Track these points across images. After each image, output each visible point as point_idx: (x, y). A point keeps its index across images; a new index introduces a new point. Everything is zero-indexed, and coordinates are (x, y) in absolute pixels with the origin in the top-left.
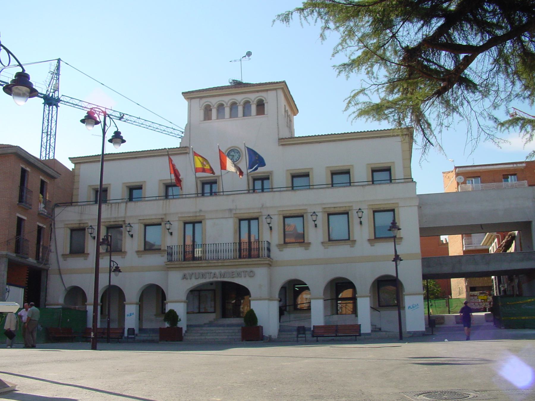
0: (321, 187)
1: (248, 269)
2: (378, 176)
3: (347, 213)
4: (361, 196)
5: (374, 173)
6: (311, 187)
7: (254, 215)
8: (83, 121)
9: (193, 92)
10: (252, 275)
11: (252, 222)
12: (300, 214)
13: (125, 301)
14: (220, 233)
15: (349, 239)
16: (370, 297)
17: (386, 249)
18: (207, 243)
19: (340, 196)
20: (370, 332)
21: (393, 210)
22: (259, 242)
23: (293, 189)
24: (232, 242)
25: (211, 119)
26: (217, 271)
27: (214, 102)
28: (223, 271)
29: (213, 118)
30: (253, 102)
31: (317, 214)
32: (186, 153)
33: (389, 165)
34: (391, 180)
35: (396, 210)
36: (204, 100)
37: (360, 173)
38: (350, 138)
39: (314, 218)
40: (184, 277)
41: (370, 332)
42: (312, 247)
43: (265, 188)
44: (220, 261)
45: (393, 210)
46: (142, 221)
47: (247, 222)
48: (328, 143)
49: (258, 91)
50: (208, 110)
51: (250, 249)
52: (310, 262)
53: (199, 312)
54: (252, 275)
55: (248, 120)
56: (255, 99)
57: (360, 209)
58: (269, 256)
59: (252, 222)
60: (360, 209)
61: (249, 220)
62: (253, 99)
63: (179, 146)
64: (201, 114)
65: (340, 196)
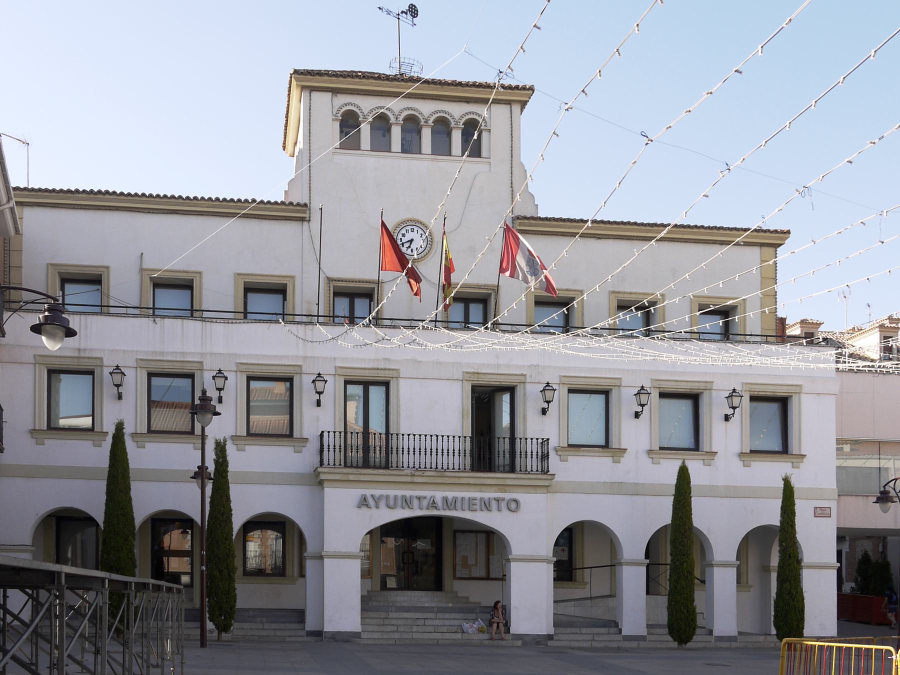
0: (126, 311)
1: (508, 496)
2: (258, 302)
3: (606, 393)
5: (250, 295)
6: (105, 309)
7: (382, 376)
9: (319, 73)
10: (514, 506)
11: (373, 390)
14: (434, 414)
15: (290, 435)
16: (712, 565)
17: (771, 473)
18: (529, 436)
19: (269, 343)
21: (606, 393)
22: (346, 433)
23: (245, 317)
25: (358, 148)
26: (439, 495)
27: (366, 106)
29: (363, 147)
30: (457, 123)
31: (226, 374)
32: (302, 219)
36: (342, 99)
37: (219, 291)
38: (560, 230)
39: (117, 378)
40: (363, 502)
42: (627, 459)
44: (447, 474)
45: (290, 380)
46: (243, 368)
48: (692, 244)
49: (468, 100)
50: (349, 122)
51: (366, 448)
52: (617, 488)
54: (514, 506)
55: (443, 164)
56: (371, 111)
58: (545, 471)
59: (373, 390)
61: (366, 385)
62: (457, 118)
63: (280, 198)
64: (330, 131)
65: (269, 343)
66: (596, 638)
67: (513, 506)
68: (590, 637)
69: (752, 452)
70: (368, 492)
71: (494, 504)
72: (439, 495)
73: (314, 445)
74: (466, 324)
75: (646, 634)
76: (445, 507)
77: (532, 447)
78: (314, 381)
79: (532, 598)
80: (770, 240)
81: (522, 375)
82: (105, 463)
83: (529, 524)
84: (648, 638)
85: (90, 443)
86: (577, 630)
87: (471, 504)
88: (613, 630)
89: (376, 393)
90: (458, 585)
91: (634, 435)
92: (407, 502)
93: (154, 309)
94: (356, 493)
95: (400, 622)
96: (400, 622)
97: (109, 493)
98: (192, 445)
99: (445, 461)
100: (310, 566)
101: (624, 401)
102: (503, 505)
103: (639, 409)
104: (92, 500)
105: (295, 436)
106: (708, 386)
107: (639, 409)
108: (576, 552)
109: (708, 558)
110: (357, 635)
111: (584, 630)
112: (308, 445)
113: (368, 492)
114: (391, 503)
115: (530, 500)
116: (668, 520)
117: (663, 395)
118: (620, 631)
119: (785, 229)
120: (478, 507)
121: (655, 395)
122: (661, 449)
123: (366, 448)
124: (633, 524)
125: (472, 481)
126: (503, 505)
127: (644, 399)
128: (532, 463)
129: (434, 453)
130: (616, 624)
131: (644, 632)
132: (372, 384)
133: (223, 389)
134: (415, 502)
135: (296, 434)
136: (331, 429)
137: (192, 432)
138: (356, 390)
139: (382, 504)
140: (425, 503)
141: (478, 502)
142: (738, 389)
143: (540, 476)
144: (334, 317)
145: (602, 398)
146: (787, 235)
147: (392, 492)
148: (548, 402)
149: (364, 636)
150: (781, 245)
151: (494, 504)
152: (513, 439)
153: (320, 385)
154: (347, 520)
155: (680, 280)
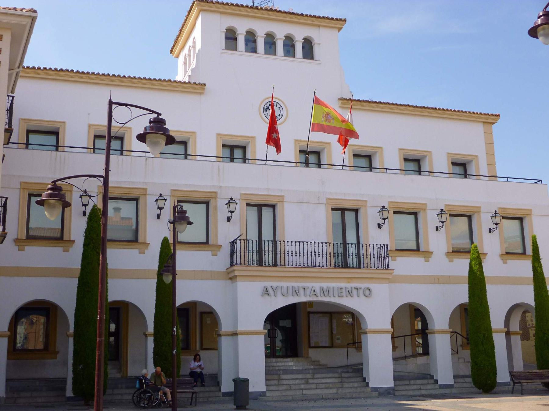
3: (137, 200)
4: (437, 191)
8: (533, 32)
11: (264, 210)
12: (202, 199)
13: (427, 329)
14: (305, 226)
18: (286, 240)
20: (391, 384)
21: (521, 219)
24: (332, 242)
26: (317, 285)
28: (325, 285)
33: (55, 125)
34: (186, 156)
35: (141, 202)
41: (391, 384)
43: (125, 148)
47: (256, 208)
53: (332, 346)
57: (161, 195)
59: (264, 210)
60: (161, 195)
61: (260, 207)
66: (422, 388)
67: (367, 292)
68: (418, 387)
69: (397, 250)
70: (268, 284)
71: (355, 292)
72: (317, 285)
73: (226, 250)
74: (307, 164)
75: (453, 383)
76: (322, 294)
77: (374, 251)
78: (157, 200)
79: (379, 359)
80: (489, 120)
81: (143, 189)
82: (531, 274)
83: (376, 307)
84: (456, 385)
85: (60, 249)
86: (407, 382)
87: (340, 292)
88: (432, 381)
89: (267, 214)
90: (313, 353)
91: (437, 242)
92: (296, 292)
93: (94, 149)
94: (258, 286)
95: (291, 382)
96: (291, 382)
97: (536, 290)
98: (210, 252)
99: (319, 260)
100: (225, 343)
101: (430, 219)
102: (361, 292)
103: (229, 215)
104: (64, 295)
105: (527, 253)
106: (424, 207)
107: (229, 215)
108: (412, 324)
109: (363, 327)
110: (264, 394)
111: (412, 382)
112: (222, 250)
113: (268, 284)
114: (285, 291)
115: (380, 290)
116: (465, 299)
117: (395, 212)
118: (436, 382)
119: (497, 114)
120: (344, 294)
121: (391, 212)
122: (453, 252)
123: (260, 252)
124: (442, 304)
125: (375, 276)
126: (361, 292)
127: (232, 207)
128: (374, 261)
129: (294, 254)
130: (432, 377)
131: (452, 382)
132: (264, 207)
133: (87, 205)
134: (302, 291)
135: (66, 238)
136: (325, 241)
137: (524, 253)
138: (253, 211)
139: (279, 293)
140: (308, 292)
141: (344, 290)
142: (386, 206)
143: (244, 268)
144: (266, 160)
145: (204, 206)
146: (498, 117)
147: (285, 284)
148: (232, 212)
149: (268, 394)
150: (494, 123)
151: (355, 292)
152: (275, 242)
153: (161, 203)
154: (246, 308)
155: (441, 141)
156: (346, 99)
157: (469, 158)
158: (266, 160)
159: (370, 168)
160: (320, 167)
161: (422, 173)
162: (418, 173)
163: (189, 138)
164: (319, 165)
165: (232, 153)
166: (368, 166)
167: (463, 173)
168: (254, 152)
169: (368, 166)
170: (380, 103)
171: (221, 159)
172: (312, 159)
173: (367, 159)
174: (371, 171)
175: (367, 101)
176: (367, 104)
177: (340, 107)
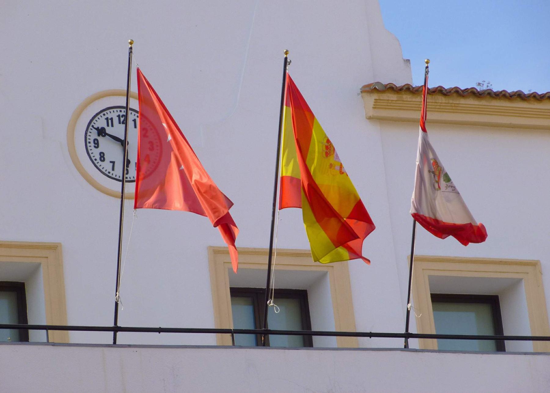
74: (261, 336)
156: (391, 89)
157: (510, 273)
158: (116, 329)
159: (499, 341)
160: (308, 344)
161: (316, 339)
162: (491, 344)
163: (35, 270)
164: (306, 336)
165: (260, 314)
166: (296, 328)
167: (489, 331)
168: (59, 300)
169: (296, 328)
170: (519, 96)
171: (433, 343)
172: (278, 314)
173: (485, 311)
174: (500, 348)
175: (473, 93)
176: (471, 102)
177: (370, 118)
